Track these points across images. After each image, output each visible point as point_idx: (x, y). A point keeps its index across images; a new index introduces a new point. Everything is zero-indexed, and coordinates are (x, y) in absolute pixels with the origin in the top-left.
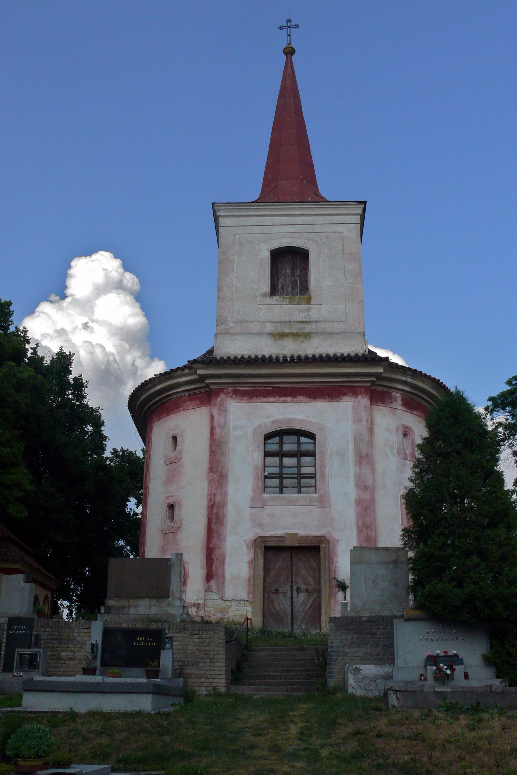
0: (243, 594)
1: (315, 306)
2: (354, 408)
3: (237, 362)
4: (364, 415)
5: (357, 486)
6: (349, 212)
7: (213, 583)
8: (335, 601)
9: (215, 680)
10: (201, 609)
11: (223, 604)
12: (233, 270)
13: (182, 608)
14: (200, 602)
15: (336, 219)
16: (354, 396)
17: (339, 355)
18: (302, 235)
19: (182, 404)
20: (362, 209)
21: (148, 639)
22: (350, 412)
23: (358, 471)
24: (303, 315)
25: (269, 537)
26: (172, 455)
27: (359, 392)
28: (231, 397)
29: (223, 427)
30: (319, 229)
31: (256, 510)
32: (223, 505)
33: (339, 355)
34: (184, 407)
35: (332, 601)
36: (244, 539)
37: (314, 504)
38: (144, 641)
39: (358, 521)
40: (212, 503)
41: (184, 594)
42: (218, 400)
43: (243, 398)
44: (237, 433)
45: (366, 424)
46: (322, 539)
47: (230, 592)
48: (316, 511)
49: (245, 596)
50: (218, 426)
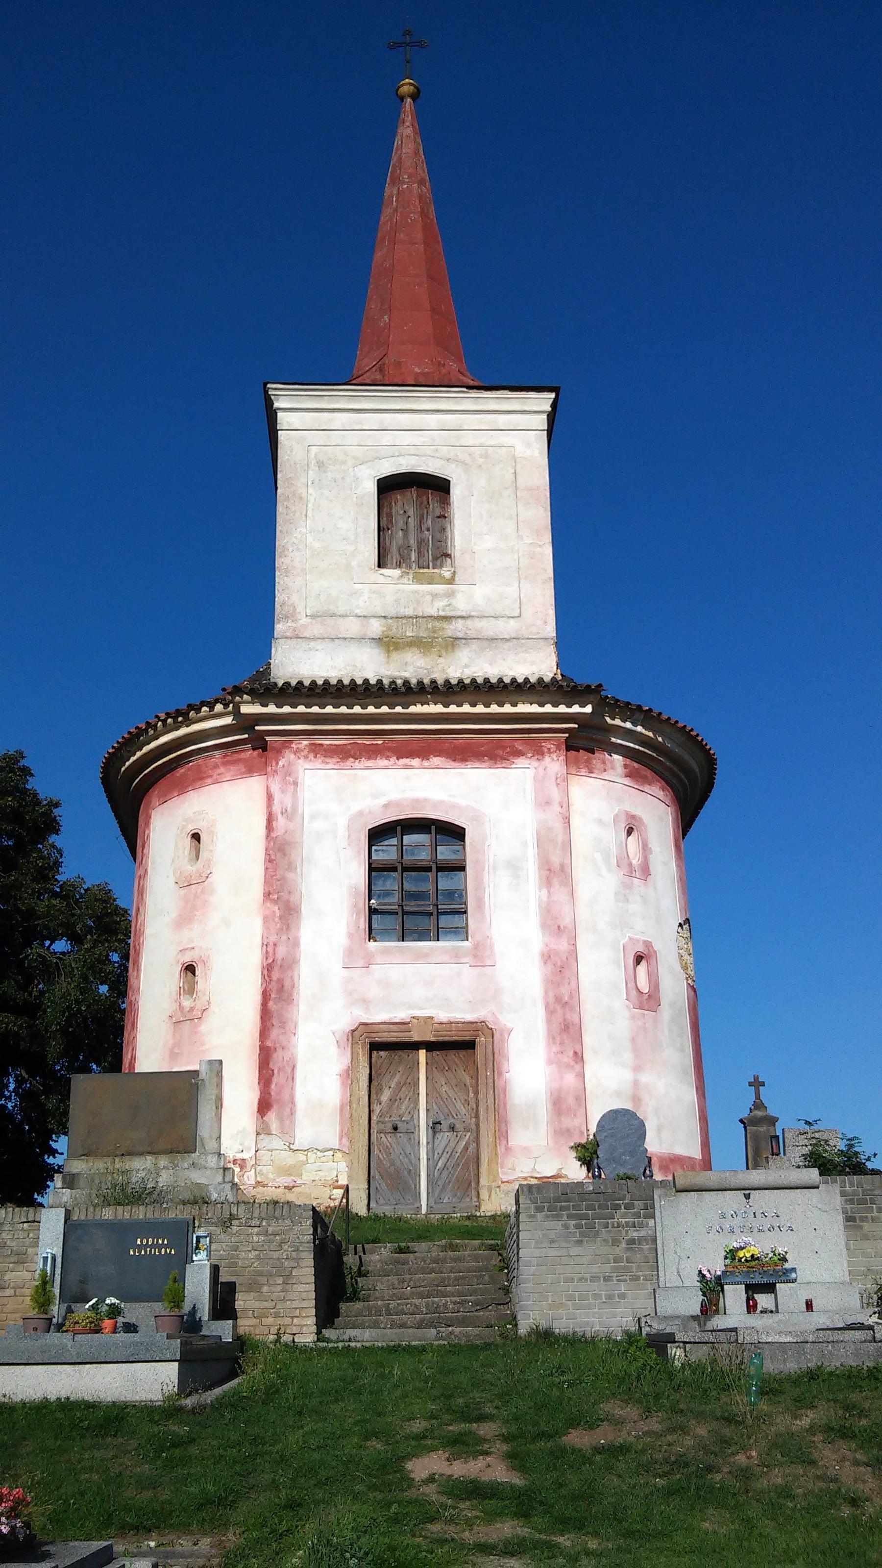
2: (535, 779)
3: (317, 691)
4: (555, 794)
5: (544, 926)
6: (527, 409)
7: (271, 1116)
8: (507, 1149)
9: (295, 1320)
11: (289, 1159)
12: (306, 516)
13: (222, 1170)
14: (245, 1155)
15: (502, 420)
17: (507, 680)
21: (160, 1242)
22: (529, 786)
24: (441, 603)
26: (190, 869)
27: (546, 750)
28: (306, 757)
29: (290, 814)
30: (469, 438)
31: (355, 973)
32: (291, 964)
33: (507, 680)
34: (215, 777)
35: (501, 1149)
38: (151, 1247)
39: (546, 992)
42: (281, 763)
43: (327, 760)
46: (480, 1027)
50: (282, 813)
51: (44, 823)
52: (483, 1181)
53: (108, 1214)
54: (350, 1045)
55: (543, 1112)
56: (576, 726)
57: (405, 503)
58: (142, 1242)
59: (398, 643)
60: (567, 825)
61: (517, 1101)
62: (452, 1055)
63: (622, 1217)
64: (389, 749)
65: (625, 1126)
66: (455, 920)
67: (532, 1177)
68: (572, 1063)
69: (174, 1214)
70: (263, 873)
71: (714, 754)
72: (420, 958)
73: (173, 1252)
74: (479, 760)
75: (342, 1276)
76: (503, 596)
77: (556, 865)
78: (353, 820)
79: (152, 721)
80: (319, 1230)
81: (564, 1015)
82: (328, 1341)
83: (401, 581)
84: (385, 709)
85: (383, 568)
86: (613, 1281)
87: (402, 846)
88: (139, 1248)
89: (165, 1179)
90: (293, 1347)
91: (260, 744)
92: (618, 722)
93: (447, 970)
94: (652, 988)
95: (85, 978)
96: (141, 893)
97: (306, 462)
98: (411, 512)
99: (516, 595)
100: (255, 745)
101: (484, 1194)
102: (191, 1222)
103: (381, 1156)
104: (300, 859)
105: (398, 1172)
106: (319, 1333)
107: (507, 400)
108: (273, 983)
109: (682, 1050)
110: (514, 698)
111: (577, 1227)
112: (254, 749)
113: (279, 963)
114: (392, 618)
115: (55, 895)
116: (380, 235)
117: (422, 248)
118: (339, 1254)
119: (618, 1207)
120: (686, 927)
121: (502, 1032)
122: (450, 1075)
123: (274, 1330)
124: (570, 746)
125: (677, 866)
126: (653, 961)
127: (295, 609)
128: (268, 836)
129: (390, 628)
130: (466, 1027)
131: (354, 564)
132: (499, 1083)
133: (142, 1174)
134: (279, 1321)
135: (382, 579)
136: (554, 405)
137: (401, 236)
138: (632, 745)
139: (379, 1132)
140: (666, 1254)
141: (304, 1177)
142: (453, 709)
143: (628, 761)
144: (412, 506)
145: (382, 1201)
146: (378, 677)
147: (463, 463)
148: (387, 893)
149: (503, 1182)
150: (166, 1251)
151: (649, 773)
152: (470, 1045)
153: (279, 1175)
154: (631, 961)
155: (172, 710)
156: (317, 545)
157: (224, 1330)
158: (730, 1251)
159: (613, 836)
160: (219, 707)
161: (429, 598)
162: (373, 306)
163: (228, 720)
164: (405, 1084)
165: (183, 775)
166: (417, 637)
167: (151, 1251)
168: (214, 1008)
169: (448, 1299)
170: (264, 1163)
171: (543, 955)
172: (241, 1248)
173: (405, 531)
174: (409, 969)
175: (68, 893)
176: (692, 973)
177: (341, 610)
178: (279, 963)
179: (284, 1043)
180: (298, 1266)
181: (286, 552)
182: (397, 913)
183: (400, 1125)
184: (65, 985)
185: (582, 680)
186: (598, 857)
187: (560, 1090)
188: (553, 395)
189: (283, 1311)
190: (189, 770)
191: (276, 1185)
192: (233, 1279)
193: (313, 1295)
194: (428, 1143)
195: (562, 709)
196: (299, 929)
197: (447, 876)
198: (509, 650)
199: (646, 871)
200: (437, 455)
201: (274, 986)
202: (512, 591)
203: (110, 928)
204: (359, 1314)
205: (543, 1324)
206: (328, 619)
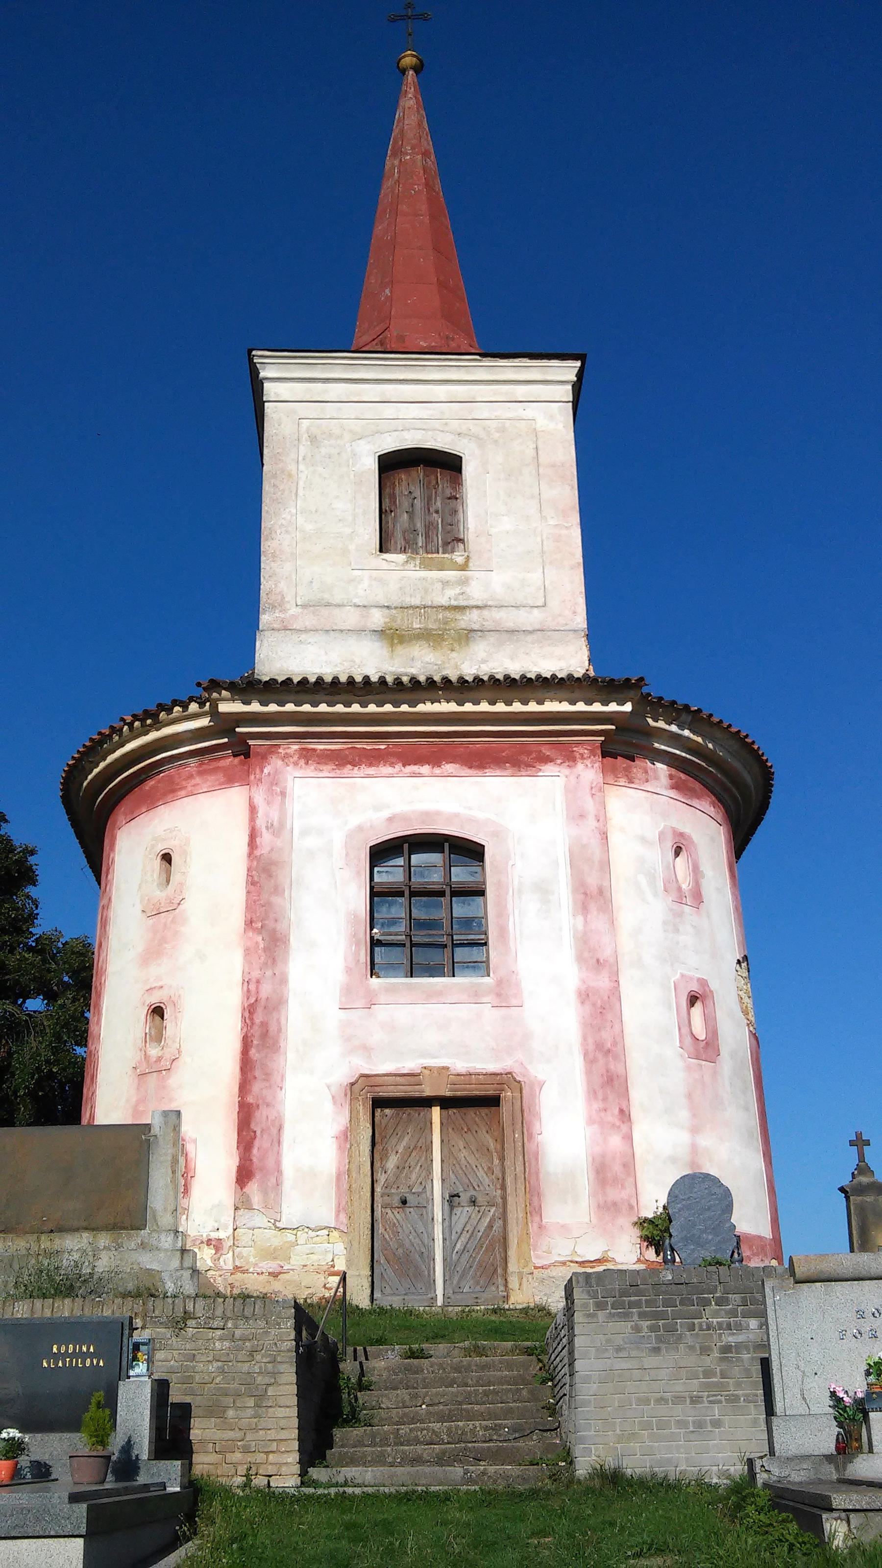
0: (324, 1210)
1: (477, 574)
2: (567, 790)
4: (590, 805)
5: (580, 959)
6: (549, 378)
7: (253, 1188)
9: (271, 1456)
11: (275, 1239)
13: (179, 1253)
14: (221, 1235)
15: (521, 391)
16: (567, 764)
18: (446, 424)
20: (576, 371)
21: (84, 1349)
23: (580, 927)
24: (451, 592)
26: (160, 895)
27: (578, 756)
28: (296, 764)
29: (277, 829)
30: (483, 411)
32: (277, 1004)
34: (189, 789)
35: (533, 1228)
37: (484, 1000)
39: (585, 1038)
40: (252, 1000)
41: (184, 1217)
42: (266, 771)
43: (325, 767)
44: (310, 842)
46: (505, 1079)
48: (489, 1014)
51: (18, 871)
52: (512, 1267)
53: (21, 1310)
54: (348, 1101)
55: (584, 1182)
56: (614, 727)
57: (410, 484)
58: (59, 1349)
59: (403, 636)
60: (604, 841)
62: (471, 1113)
63: (713, 1316)
65: (701, 1194)
66: (475, 954)
67: (571, 1262)
68: (618, 1123)
69: (111, 1310)
70: (244, 899)
71: (771, 767)
72: (431, 997)
73: (101, 1364)
74: (500, 767)
75: (338, 1390)
76: (525, 580)
77: (594, 890)
78: (350, 836)
79: (117, 724)
80: (304, 1333)
82: (315, 1484)
83: (406, 568)
84: (388, 708)
86: (702, 1402)
88: (57, 1357)
89: (104, 1264)
90: (268, 1496)
91: (242, 749)
92: (661, 724)
93: (464, 1011)
94: (710, 1035)
95: (58, 1037)
96: (105, 923)
97: (296, 437)
98: (417, 493)
100: (236, 749)
102: (127, 1323)
103: (387, 1236)
104: (288, 881)
105: (407, 1255)
106: (303, 1474)
107: (526, 369)
108: (256, 1028)
109: (747, 1109)
110: (540, 694)
111: (652, 1329)
112: (235, 756)
113: (263, 1002)
114: (396, 608)
115: (30, 949)
116: (380, 208)
117: (427, 220)
118: (334, 1360)
119: (707, 1303)
120: (744, 965)
122: (469, 1137)
123: (242, 1470)
124: (607, 752)
125: (733, 894)
126: (709, 1002)
127: (283, 598)
128: (250, 854)
129: (393, 619)
131: (352, 547)
132: (530, 1147)
133: (76, 1256)
134: (250, 1458)
135: (385, 565)
136: (580, 374)
137: (404, 207)
138: (678, 752)
139: (384, 1206)
140: (784, 1369)
141: (292, 1261)
142: (469, 707)
144: (419, 487)
145: (388, 1291)
146: (380, 674)
147: (477, 438)
148: (393, 921)
149: (536, 1268)
150: (92, 1362)
151: (697, 786)
152: (492, 1102)
155: (139, 712)
156: (309, 527)
157: (169, 1476)
158: (875, 1363)
159: (658, 856)
160: (194, 707)
161: (439, 586)
162: (372, 280)
163: (204, 722)
164: (415, 1147)
165: (152, 787)
166: (426, 629)
167: (71, 1361)
168: (185, 1058)
169: (477, 1423)
170: (243, 1244)
171: (579, 994)
172: (198, 1358)
173: (411, 514)
174: (419, 1010)
175: (44, 948)
176: (753, 1019)
177: (337, 599)
180: (275, 1383)
181: (273, 535)
182: (404, 945)
183: (410, 1198)
184: (34, 1044)
185: (619, 675)
186: (643, 880)
187: (603, 1156)
188: (578, 364)
189: (254, 1442)
190: (159, 782)
191: (259, 1270)
192: (187, 1399)
193: (295, 1422)
194: (444, 1220)
195: (597, 707)
196: (286, 962)
198: (533, 644)
199: (698, 897)
200: (446, 429)
201: (256, 1031)
202: (535, 577)
203: (76, 976)
204: (360, 1443)
205: (610, 1463)
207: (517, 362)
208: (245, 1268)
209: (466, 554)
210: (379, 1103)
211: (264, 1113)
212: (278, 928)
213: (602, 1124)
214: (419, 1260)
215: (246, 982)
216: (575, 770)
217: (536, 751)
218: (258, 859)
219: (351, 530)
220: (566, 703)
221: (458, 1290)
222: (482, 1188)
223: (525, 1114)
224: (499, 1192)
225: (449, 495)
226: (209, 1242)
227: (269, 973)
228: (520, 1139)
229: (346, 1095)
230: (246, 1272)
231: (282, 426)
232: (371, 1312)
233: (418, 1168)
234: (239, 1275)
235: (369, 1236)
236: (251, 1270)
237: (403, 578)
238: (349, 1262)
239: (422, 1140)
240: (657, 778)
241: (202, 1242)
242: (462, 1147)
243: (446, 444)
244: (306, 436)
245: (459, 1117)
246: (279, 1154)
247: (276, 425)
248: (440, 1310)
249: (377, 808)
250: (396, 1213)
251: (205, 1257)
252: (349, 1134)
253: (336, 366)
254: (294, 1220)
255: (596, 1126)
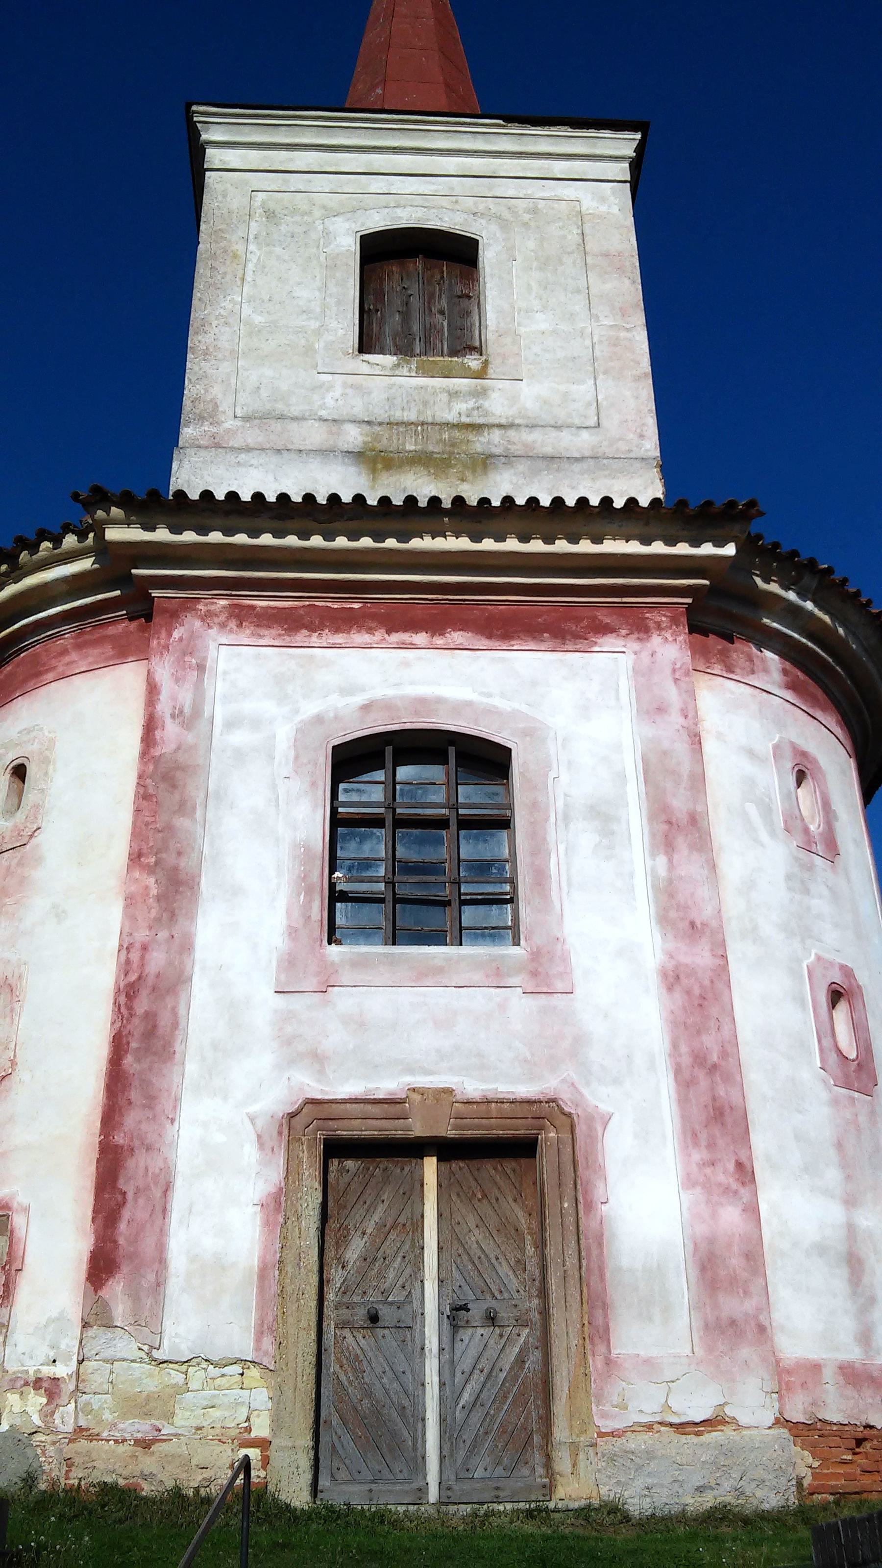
0: (238, 1334)
1: (500, 384)
4: (673, 695)
5: (664, 920)
7: (116, 1290)
10: (64, 1398)
11: (149, 1379)
12: (243, 279)
14: (62, 1370)
15: (560, 168)
16: (636, 635)
18: (457, 202)
19: (54, 662)
20: (634, 144)
22: (625, 684)
23: (662, 872)
25: (344, 1101)
27: (652, 625)
28: (223, 626)
29: (189, 718)
30: (509, 188)
32: (173, 983)
34: (60, 669)
35: (596, 1363)
36: (248, 1111)
37: (511, 981)
39: (675, 1046)
40: (133, 977)
42: (176, 634)
43: (263, 632)
44: (240, 738)
45: (681, 720)
46: (545, 1111)
47: (184, 1325)
48: (519, 1005)
49: (242, 1342)
50: (173, 716)
52: (561, 1432)
54: (284, 1144)
55: (681, 1286)
57: (407, 280)
59: (392, 459)
60: (697, 746)
61: (625, 1262)
62: (489, 1169)
64: (374, 617)
68: (735, 1186)
72: (425, 976)
74: (534, 638)
76: (569, 376)
78: (302, 731)
81: (712, 1089)
85: (369, 352)
87: (394, 783)
92: (774, 587)
93: (479, 999)
94: (862, 1049)
99: (590, 396)
100: (130, 605)
101: (562, 1462)
103: (343, 1378)
104: (202, 795)
108: (136, 1021)
112: (131, 619)
113: (151, 980)
114: (380, 424)
121: (590, 1119)
122: (485, 1208)
127: (216, 406)
129: (377, 438)
130: (519, 1111)
131: (319, 345)
132: (588, 1224)
135: (365, 368)
136: (640, 149)
138: (796, 636)
141: (178, 1421)
143: (788, 665)
144: (416, 284)
145: (343, 1475)
148: (367, 863)
149: (601, 1435)
151: (819, 693)
152: (523, 1148)
153: (124, 1416)
154: (823, 998)
156: (258, 319)
159: (774, 781)
160: (70, 541)
161: (444, 397)
163: (86, 564)
168: (22, 1074)
171: (664, 974)
173: (406, 316)
174: (406, 996)
177: (295, 411)
178: (151, 980)
179: (151, 1138)
182: (382, 901)
183: (385, 1312)
186: (753, 810)
187: (712, 1241)
188: (638, 136)
194: (441, 1350)
195: (683, 549)
196: (192, 917)
197: (477, 838)
199: (832, 848)
200: (458, 208)
201: (137, 1026)
202: (584, 390)
206: (272, 422)
207: (554, 131)
208: (95, 1431)
209: (483, 358)
210: (335, 1149)
211: (142, 1165)
212: (182, 865)
213: (708, 1186)
214: (399, 1420)
215: (125, 948)
216: (649, 645)
217: (588, 618)
218: (156, 760)
219: (318, 324)
220: (637, 543)
221: (464, 1474)
222: (506, 1295)
223: (580, 1169)
224: (536, 1301)
225: (459, 293)
226: (37, 1384)
227: (163, 935)
228: (572, 1211)
229: (280, 1133)
230: (94, 1437)
231: (228, 199)
232: (309, 1516)
233: (399, 1259)
234: (83, 1444)
235: (313, 1378)
236: (105, 1435)
237: (392, 386)
238: (277, 1423)
239: (408, 1210)
240: (766, 670)
241: (26, 1384)
242: (472, 1225)
243: (455, 224)
244: (260, 211)
245: (468, 1174)
246: (163, 1233)
247: (220, 198)
248: (432, 1511)
249: (346, 691)
250: (359, 1336)
251: (29, 1409)
252: (283, 1199)
253: (309, 128)
254: (183, 1347)
255: (698, 1190)
